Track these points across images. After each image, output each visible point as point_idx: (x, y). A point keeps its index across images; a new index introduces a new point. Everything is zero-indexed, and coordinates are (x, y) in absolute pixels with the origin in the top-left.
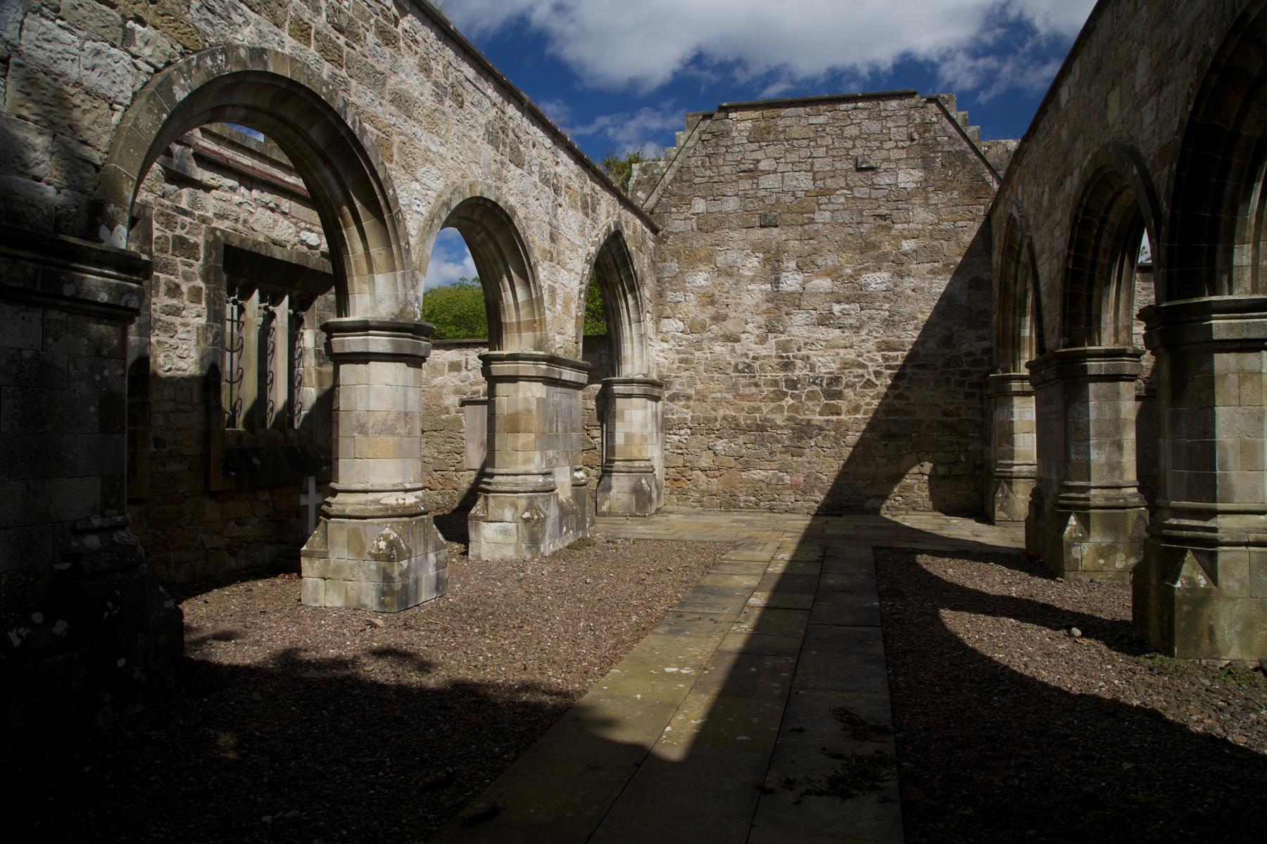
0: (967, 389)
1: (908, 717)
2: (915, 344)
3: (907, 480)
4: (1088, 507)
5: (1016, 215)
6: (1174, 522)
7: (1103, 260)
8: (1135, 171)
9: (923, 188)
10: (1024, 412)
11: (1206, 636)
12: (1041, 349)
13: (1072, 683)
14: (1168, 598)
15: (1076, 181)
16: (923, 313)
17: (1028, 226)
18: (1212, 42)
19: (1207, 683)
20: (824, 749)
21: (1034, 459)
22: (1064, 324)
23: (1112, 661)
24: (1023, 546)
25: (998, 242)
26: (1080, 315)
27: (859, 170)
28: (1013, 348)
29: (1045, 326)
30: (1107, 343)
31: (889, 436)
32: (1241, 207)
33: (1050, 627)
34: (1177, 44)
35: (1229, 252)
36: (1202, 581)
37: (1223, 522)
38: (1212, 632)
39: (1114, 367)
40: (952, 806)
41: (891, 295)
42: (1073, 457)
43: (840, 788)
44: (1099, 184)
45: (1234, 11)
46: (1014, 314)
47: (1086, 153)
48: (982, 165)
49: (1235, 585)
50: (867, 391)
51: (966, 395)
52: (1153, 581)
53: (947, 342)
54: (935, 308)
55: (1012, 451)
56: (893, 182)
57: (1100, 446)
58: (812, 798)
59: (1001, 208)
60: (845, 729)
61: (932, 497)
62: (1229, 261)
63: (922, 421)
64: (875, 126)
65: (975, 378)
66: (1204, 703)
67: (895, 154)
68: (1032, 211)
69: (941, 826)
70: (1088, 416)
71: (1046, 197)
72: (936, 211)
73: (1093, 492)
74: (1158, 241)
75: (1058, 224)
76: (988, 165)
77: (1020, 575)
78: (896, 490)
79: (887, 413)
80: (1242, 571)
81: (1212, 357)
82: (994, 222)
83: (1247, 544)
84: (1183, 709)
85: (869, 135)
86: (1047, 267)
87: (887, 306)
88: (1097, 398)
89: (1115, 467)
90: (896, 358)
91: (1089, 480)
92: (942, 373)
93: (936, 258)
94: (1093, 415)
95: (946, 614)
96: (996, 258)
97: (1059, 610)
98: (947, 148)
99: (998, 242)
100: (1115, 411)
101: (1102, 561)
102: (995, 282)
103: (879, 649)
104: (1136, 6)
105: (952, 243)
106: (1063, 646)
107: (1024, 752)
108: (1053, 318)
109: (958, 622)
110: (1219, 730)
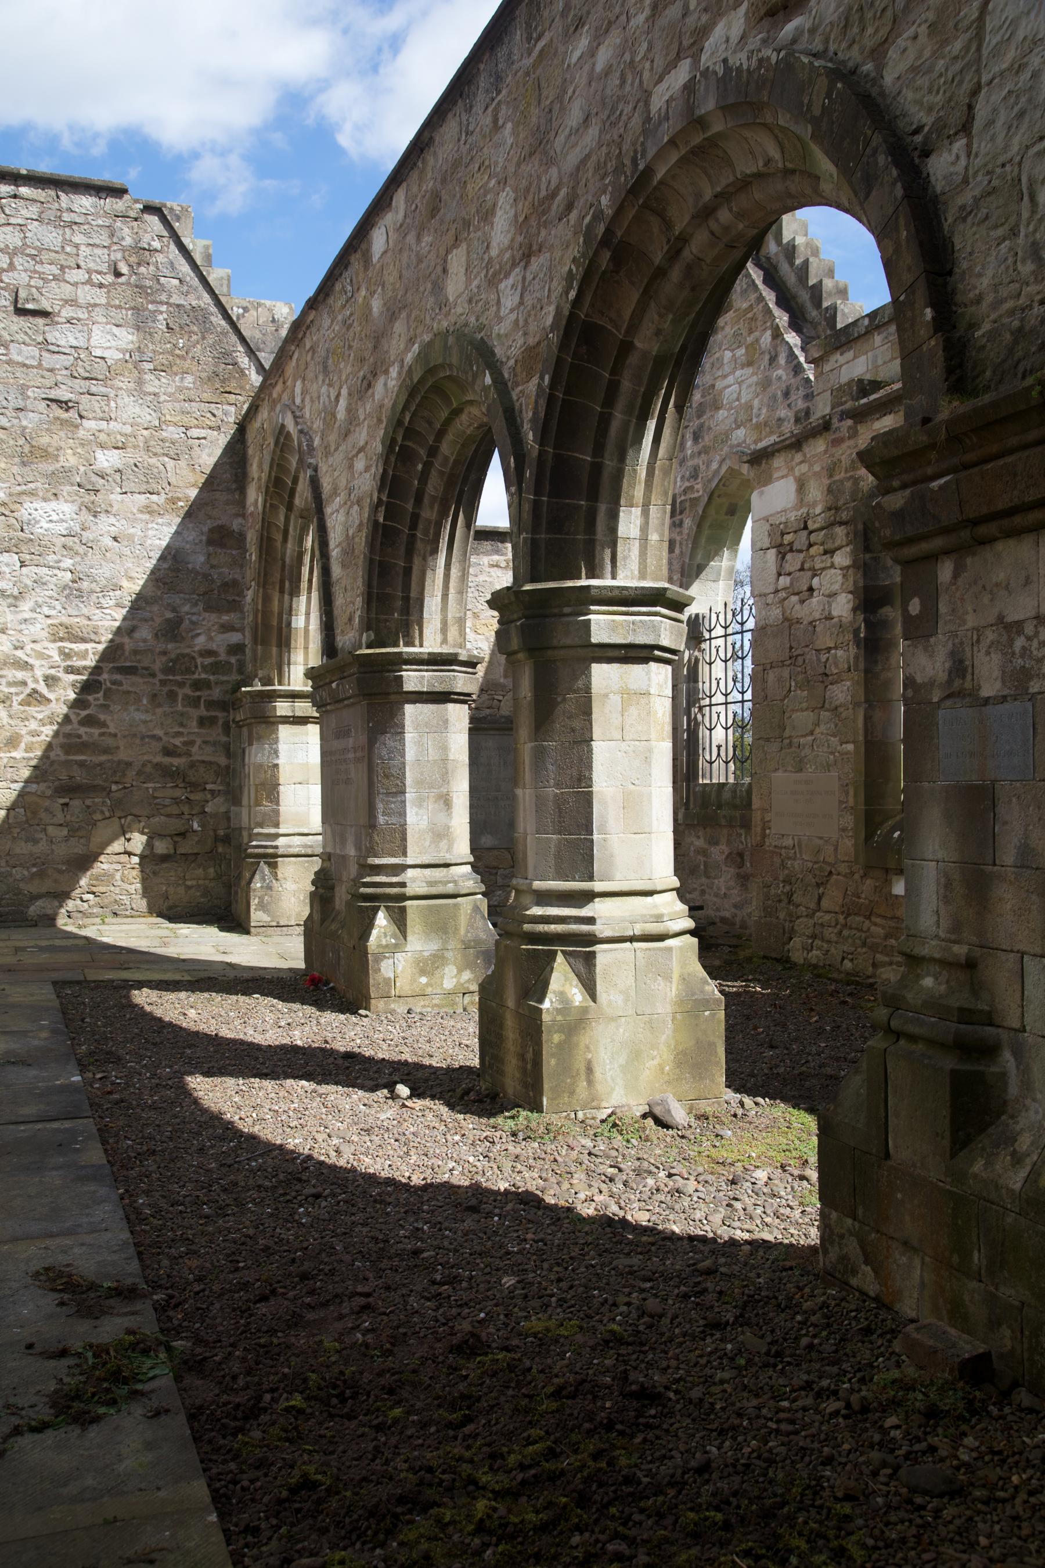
0: (203, 711)
1: (166, 1262)
2: (119, 631)
3: (104, 865)
4: (404, 898)
5: (291, 427)
6: (537, 911)
7: (429, 513)
8: (488, 380)
9: (135, 359)
10: (298, 755)
11: (583, 1077)
12: (329, 648)
13: (411, 1170)
14: (532, 1027)
15: (392, 383)
16: (131, 578)
17: (311, 448)
18: (605, 200)
19: (589, 1143)
20: (30, 1346)
21: (315, 821)
22: (369, 610)
23: (458, 1129)
24: (302, 965)
25: (258, 469)
26: (391, 595)
27: (21, 312)
28: (279, 646)
29: (337, 612)
30: (431, 643)
31: (69, 789)
32: (631, 453)
33: (362, 1087)
34: (553, 195)
35: (613, 517)
36: (577, 995)
37: (598, 908)
38: (590, 1070)
39: (442, 681)
40: (267, 1397)
41: (77, 542)
42: (381, 819)
43: (74, 1409)
44: (429, 393)
45: (634, 161)
46: (282, 591)
47: (411, 341)
48: (234, 338)
49: (617, 999)
50: (32, 710)
51: (202, 722)
52: (511, 1003)
53: (172, 630)
54: (152, 572)
55: (277, 813)
56: (82, 343)
57: (420, 803)
58: (27, 1440)
59: (263, 414)
60: (62, 1304)
61: (146, 892)
62: (613, 530)
63: (129, 764)
64: (51, 237)
65: (216, 693)
66: (588, 1173)
67: (86, 295)
68: (318, 425)
69: (257, 1434)
70: (403, 756)
71: (343, 403)
72: (156, 407)
73: (410, 873)
74: (520, 490)
75: (361, 450)
76: (243, 339)
77: (303, 1011)
78: (83, 882)
79: (68, 748)
80: (626, 979)
81: (588, 668)
82: (251, 435)
83: (632, 939)
84: (566, 1185)
85: (40, 250)
86: (341, 517)
87: (67, 563)
88: (417, 727)
89: (441, 834)
90: (84, 655)
91: (405, 854)
92: (163, 683)
93: (154, 486)
94: (410, 753)
95: (197, 1083)
96: (254, 497)
97: (370, 1060)
98: (176, 299)
99: (258, 469)
100: (436, 746)
101: (424, 980)
102: (252, 537)
103: (95, 1155)
104: (495, 120)
105: (182, 463)
106: (388, 1113)
107: (360, 1289)
108: (350, 601)
109: (217, 1093)
110: (614, 1208)
